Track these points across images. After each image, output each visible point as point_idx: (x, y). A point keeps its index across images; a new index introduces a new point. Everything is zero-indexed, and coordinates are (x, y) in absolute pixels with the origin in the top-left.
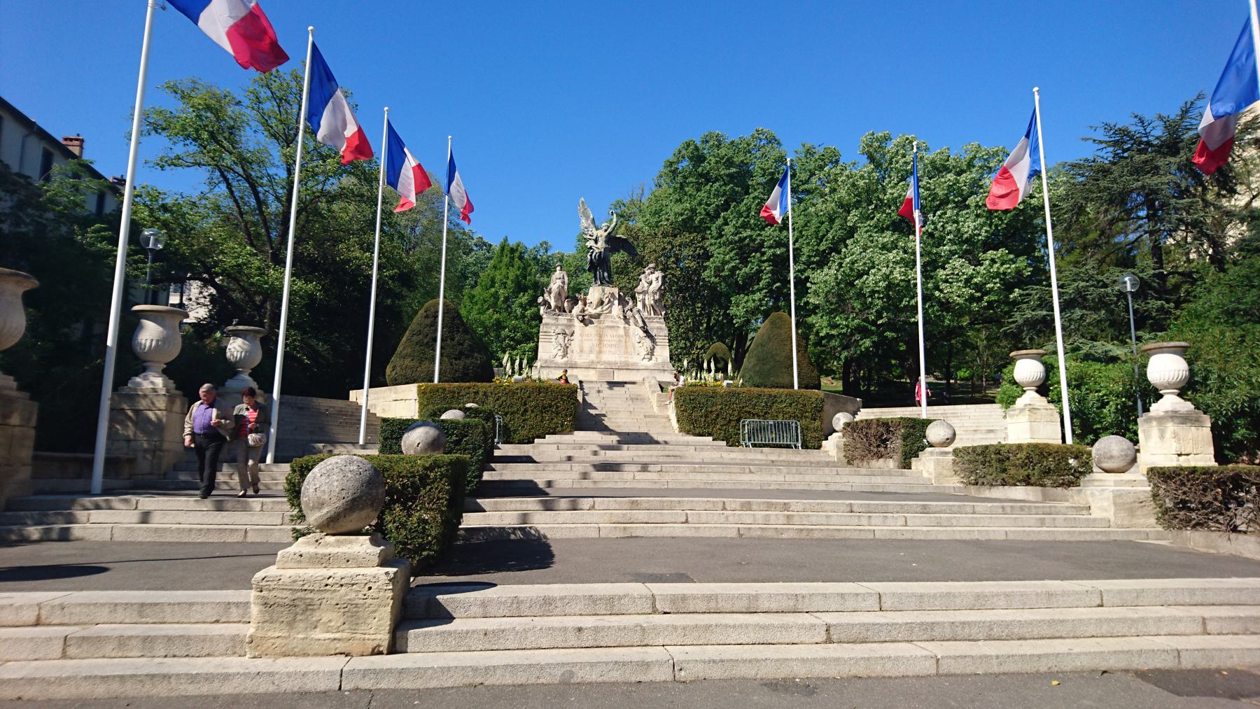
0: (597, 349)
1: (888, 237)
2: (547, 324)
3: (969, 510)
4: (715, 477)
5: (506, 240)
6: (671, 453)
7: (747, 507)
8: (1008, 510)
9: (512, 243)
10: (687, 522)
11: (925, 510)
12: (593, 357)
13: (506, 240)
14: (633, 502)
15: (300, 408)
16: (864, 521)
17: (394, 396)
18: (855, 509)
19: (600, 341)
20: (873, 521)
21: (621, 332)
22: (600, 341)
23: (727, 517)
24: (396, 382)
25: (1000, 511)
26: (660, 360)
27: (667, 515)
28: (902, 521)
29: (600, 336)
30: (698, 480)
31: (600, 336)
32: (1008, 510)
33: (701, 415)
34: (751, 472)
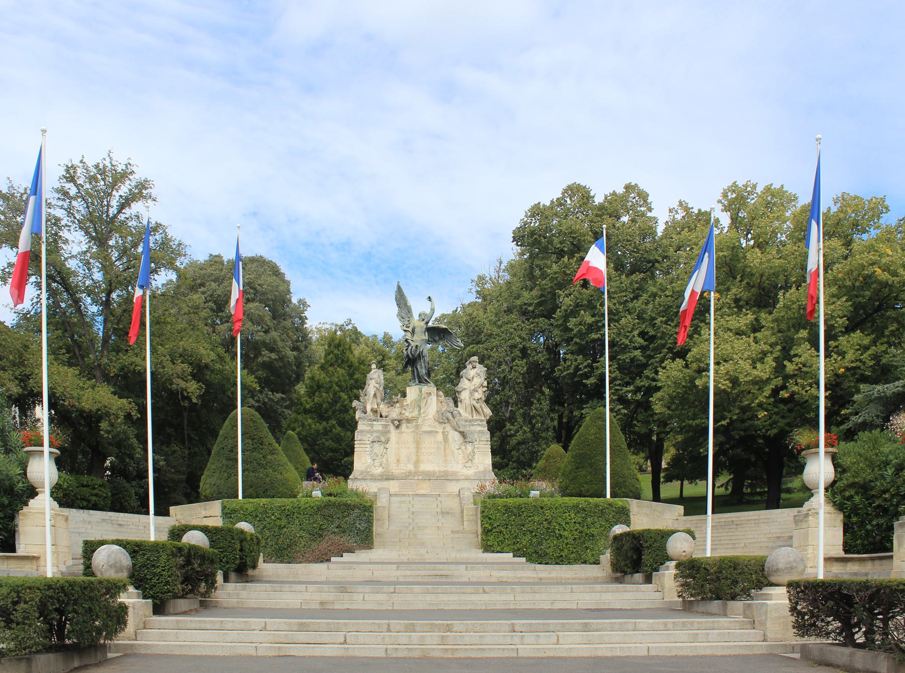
0: (414, 458)
1: (747, 318)
2: (362, 431)
3: (630, 626)
4: (444, 598)
5: (771, 185)
6: (439, 573)
7: (411, 629)
8: (670, 626)
9: (776, 186)
10: (345, 642)
11: (586, 628)
12: (411, 467)
13: (771, 185)
14: (302, 624)
15: (120, 525)
16: (517, 640)
17: (204, 513)
18: (517, 628)
19: (418, 448)
20: (526, 640)
21: (440, 437)
22: (418, 448)
23: (384, 638)
24: (207, 499)
25: (662, 627)
26: (481, 468)
27: (326, 637)
28: (554, 640)
29: (418, 444)
30: (479, 600)
31: (418, 444)
32: (670, 626)
33: (505, 529)
34: (484, 592)
